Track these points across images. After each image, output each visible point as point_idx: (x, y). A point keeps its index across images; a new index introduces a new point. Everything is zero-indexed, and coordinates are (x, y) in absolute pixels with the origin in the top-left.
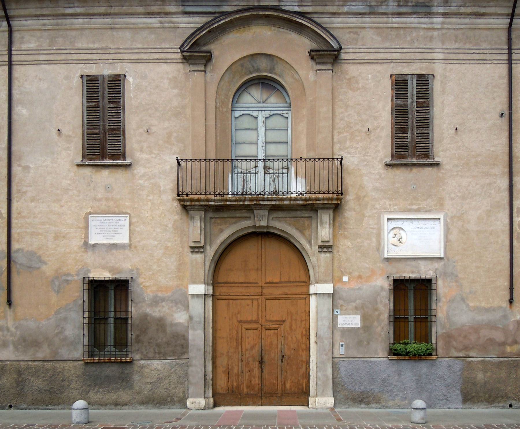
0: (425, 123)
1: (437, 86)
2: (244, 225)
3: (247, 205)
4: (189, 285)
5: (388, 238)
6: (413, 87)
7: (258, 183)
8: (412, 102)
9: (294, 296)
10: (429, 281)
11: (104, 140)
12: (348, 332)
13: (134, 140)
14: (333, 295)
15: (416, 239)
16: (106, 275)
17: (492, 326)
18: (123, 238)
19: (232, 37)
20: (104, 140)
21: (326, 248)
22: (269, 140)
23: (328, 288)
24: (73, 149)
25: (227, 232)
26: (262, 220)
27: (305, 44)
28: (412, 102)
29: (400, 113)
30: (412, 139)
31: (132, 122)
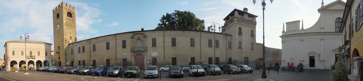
0: (155, 43)
1: (157, 39)
2: (137, 53)
3: (138, 51)
4: (256, 42)
5: (152, 54)
6: (154, 40)
7: (139, 49)
8: (154, 41)
9: (323, 34)
10: (156, 58)
11: (124, 46)
12: (148, 63)
13: (127, 46)
14: (147, 60)
15: (155, 54)
16: (124, 58)
17: (162, 62)
18: (126, 55)
19: (136, 36)
20: (124, 46)
21: (146, 55)
22: (336, 22)
23: (146, 59)
24: (121, 47)
25: (136, 54)
26: (139, 53)
27: (143, 36)
28: (154, 41)
29: (153, 42)
30: (154, 44)
31: (127, 44)
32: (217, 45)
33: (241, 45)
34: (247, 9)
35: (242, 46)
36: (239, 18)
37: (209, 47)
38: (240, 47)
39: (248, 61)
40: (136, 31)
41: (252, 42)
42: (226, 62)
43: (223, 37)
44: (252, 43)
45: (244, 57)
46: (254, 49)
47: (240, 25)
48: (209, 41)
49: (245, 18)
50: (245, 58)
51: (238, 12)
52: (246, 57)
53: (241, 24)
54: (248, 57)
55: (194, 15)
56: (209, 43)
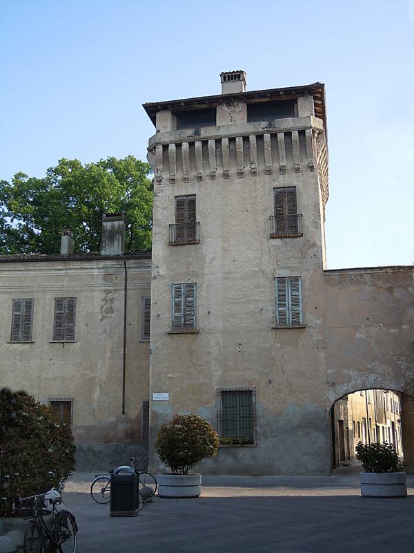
4: (334, 259)
32: (64, 328)
33: (191, 306)
34: (236, 76)
35: (200, 312)
36: (172, 147)
37: (14, 339)
38: (185, 326)
39: (249, 416)
40: (368, 266)
41: (285, 273)
42: (120, 426)
43: (107, 277)
44: (282, 280)
45: (215, 386)
46: (311, 319)
47: (186, 180)
48: (17, 305)
49: (222, 132)
50: (224, 393)
51: (174, 114)
52: (230, 387)
53: (193, 174)
54: (252, 387)
55: (65, 166)
56: (58, 317)
